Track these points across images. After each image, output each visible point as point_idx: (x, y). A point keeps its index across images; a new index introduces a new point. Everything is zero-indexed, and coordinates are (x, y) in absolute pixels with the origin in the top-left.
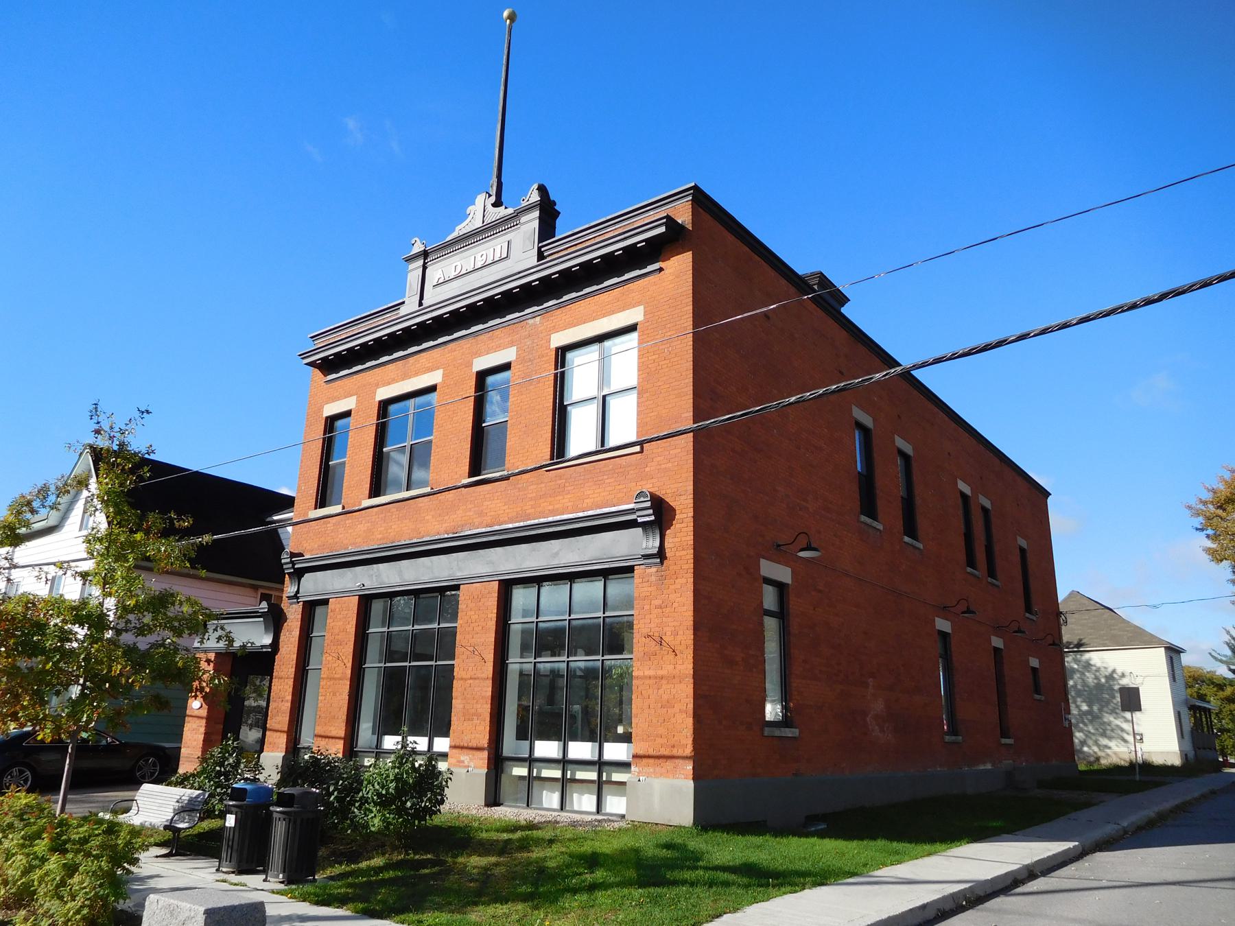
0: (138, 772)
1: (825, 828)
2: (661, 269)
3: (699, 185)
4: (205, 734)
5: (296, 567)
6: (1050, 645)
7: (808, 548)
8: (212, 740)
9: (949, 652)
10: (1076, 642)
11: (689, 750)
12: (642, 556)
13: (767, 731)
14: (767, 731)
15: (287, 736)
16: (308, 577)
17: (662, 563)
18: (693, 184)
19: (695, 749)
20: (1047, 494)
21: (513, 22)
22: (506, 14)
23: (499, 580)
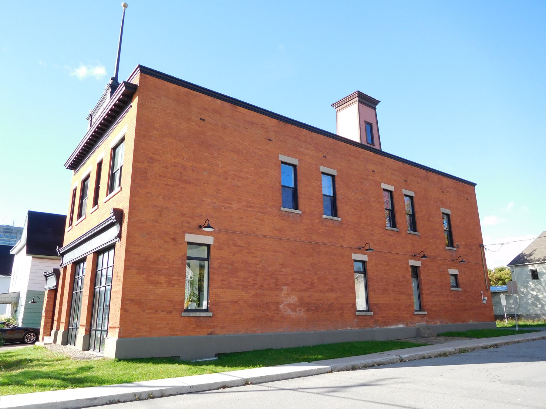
0: (26, 339)
1: (217, 359)
2: (131, 106)
3: (141, 65)
4: (44, 323)
5: (61, 253)
6: (460, 262)
7: (209, 227)
8: (47, 326)
9: (366, 270)
10: (542, 258)
11: (118, 325)
12: (115, 237)
13: (357, 313)
14: (357, 313)
15: (57, 323)
16: (65, 256)
17: (120, 239)
18: (138, 65)
19: (120, 324)
20: (474, 185)
21: (126, 8)
22: (122, 4)
23: (93, 253)
